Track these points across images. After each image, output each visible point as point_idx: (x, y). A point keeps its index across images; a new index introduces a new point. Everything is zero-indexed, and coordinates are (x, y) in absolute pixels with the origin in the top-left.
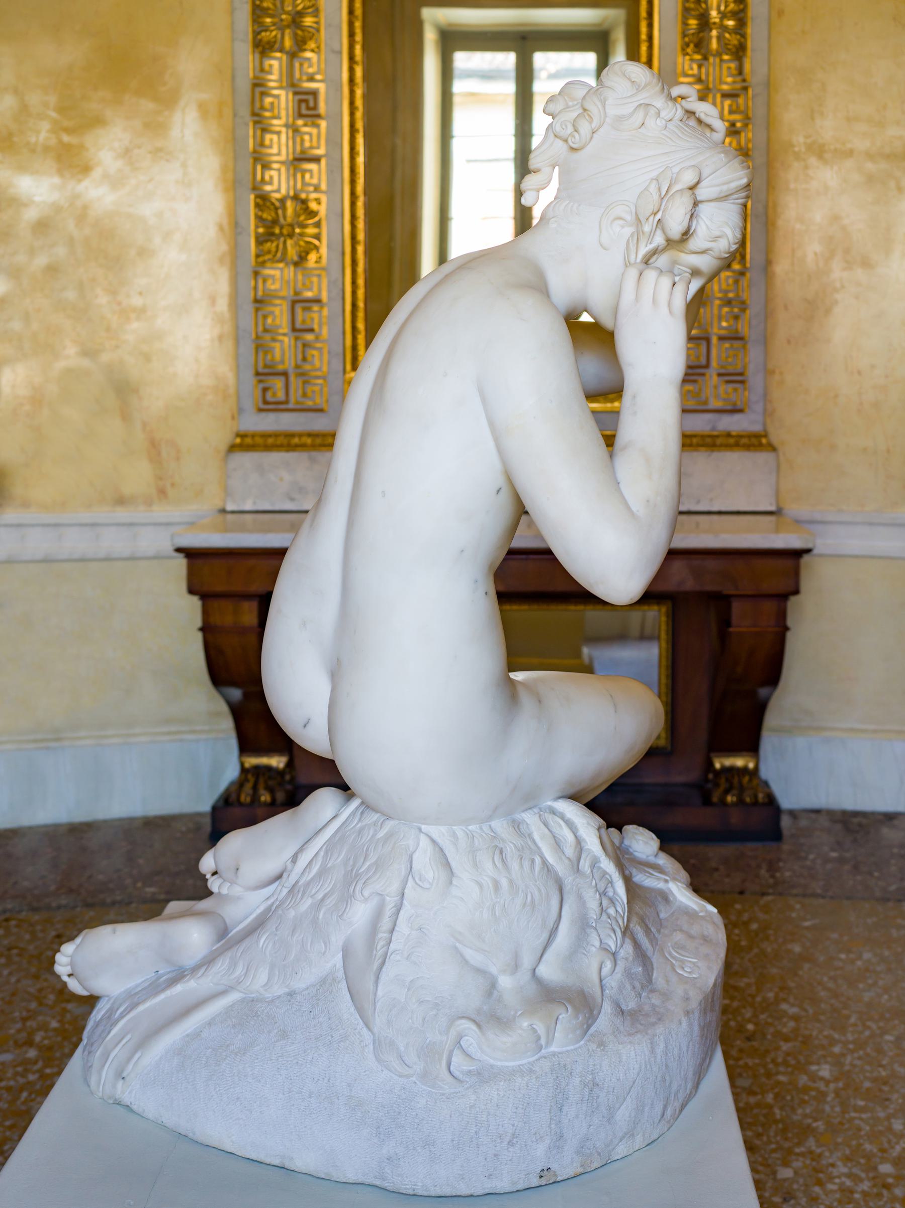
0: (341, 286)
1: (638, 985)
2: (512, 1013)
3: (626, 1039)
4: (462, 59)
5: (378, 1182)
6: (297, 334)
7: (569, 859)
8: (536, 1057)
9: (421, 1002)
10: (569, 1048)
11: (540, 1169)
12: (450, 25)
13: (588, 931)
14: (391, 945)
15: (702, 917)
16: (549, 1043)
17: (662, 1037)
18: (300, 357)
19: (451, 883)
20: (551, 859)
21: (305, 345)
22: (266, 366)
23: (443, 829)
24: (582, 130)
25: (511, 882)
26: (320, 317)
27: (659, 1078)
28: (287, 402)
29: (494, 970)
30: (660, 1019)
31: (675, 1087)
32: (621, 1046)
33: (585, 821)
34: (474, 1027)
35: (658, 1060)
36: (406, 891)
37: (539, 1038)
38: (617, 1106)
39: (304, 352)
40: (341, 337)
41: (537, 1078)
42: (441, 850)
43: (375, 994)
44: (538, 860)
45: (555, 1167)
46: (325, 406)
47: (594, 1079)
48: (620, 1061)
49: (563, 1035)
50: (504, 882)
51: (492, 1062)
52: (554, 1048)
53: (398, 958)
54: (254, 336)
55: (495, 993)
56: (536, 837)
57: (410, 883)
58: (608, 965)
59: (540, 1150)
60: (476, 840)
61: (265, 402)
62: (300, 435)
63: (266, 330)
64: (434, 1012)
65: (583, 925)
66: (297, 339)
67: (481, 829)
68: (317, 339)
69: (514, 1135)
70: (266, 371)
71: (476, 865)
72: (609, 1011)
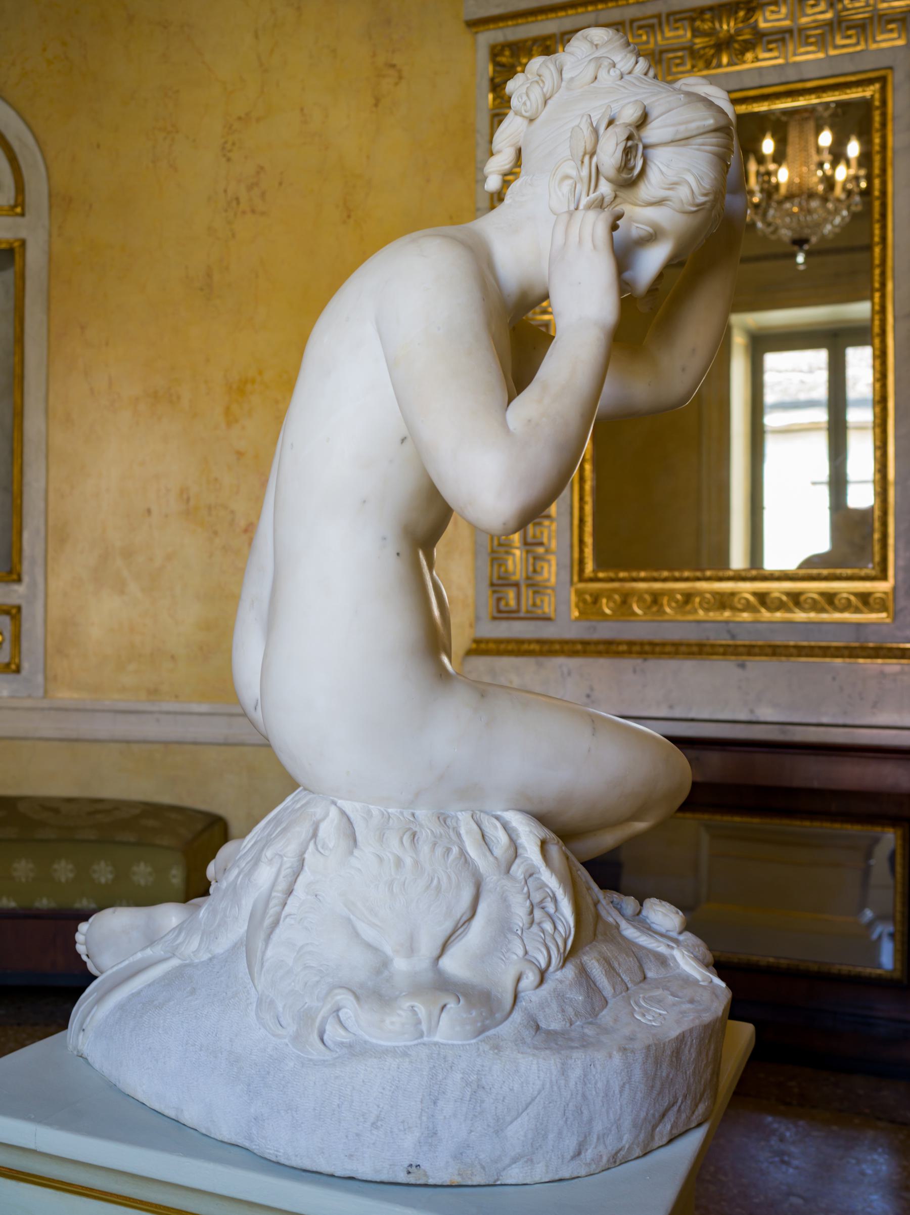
0: (569, 502)
1: (570, 1011)
2: (397, 993)
3: (529, 1050)
4: (773, 360)
5: (247, 1144)
6: (529, 548)
7: (496, 858)
8: (416, 1042)
9: (306, 967)
10: (455, 1042)
11: (408, 1163)
12: (761, 329)
13: (509, 936)
14: (286, 908)
15: (702, 986)
16: (432, 1030)
17: (579, 1062)
18: (531, 569)
19: (351, 853)
20: (473, 852)
21: (536, 558)
22: (500, 578)
23: (358, 805)
24: (532, 96)
25: (416, 863)
26: (550, 531)
27: (571, 1106)
28: (518, 611)
29: (388, 950)
30: (583, 1046)
31: (598, 1127)
32: (520, 1056)
33: (527, 829)
34: (351, 998)
35: (572, 1084)
36: (306, 856)
37: (419, 1022)
38: (508, 1119)
39: (534, 565)
40: (568, 549)
41: (411, 1062)
42: (349, 819)
43: (264, 953)
44: (455, 850)
45: (425, 1165)
46: (552, 615)
47: (479, 1080)
48: (517, 1071)
49: (450, 1026)
50: (408, 861)
51: (367, 1038)
52: (437, 1038)
53: (293, 922)
54: (489, 550)
55: (386, 973)
56: (463, 831)
57: (311, 846)
58: (530, 978)
59: (409, 1141)
60: (391, 821)
61: (499, 611)
62: (530, 642)
63: (500, 545)
64: (317, 979)
65: (503, 928)
66: (528, 552)
67: (402, 813)
68: (547, 551)
69: (378, 1118)
70: (500, 582)
71: (381, 838)
72: (519, 1021)
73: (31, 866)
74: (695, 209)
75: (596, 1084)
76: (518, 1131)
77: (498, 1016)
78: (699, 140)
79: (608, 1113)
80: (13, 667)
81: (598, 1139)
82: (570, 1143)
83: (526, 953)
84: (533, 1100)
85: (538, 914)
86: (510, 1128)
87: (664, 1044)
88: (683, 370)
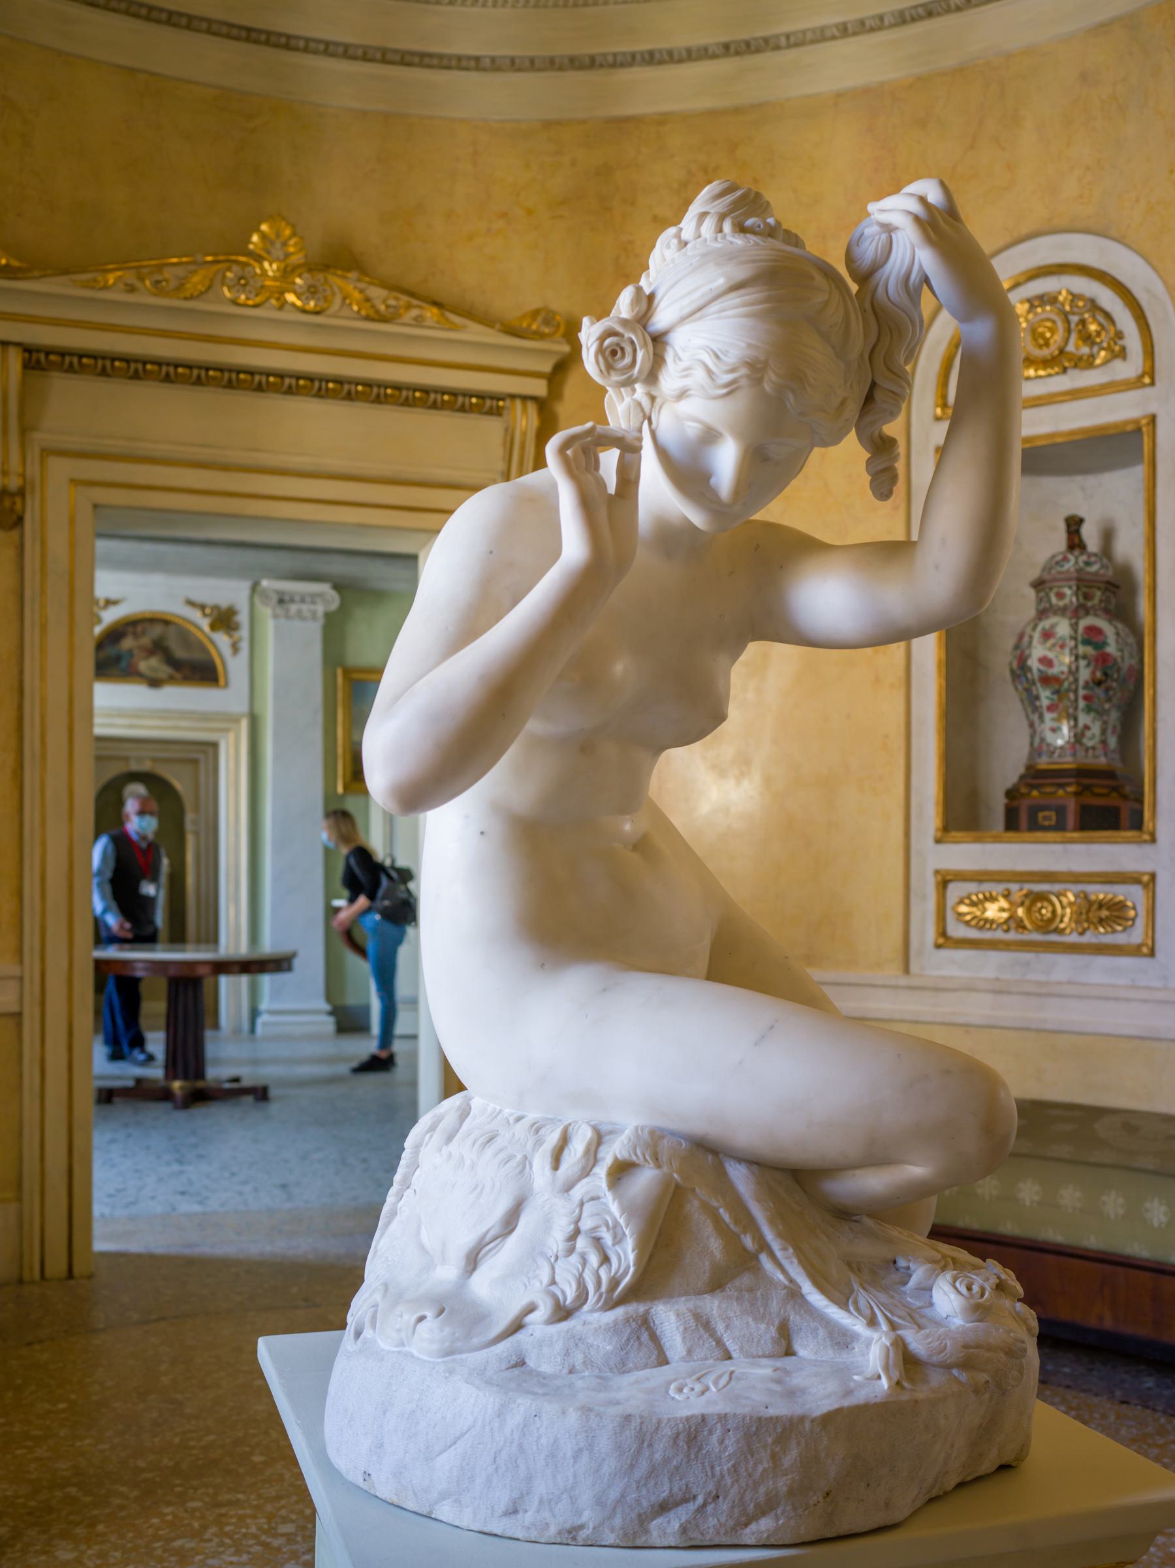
1: (578, 1358)
17: (522, 1408)
31: (541, 1488)
65: (534, 1251)
73: (1078, 1194)
74: (725, 391)
75: (539, 1437)
76: (446, 1463)
77: (475, 1341)
78: (714, 307)
79: (554, 1477)
80: (1145, 950)
81: (541, 1501)
82: (502, 1497)
83: (553, 1282)
84: (463, 1435)
85: (581, 1243)
86: (438, 1459)
87: (659, 1422)
88: (937, 567)
